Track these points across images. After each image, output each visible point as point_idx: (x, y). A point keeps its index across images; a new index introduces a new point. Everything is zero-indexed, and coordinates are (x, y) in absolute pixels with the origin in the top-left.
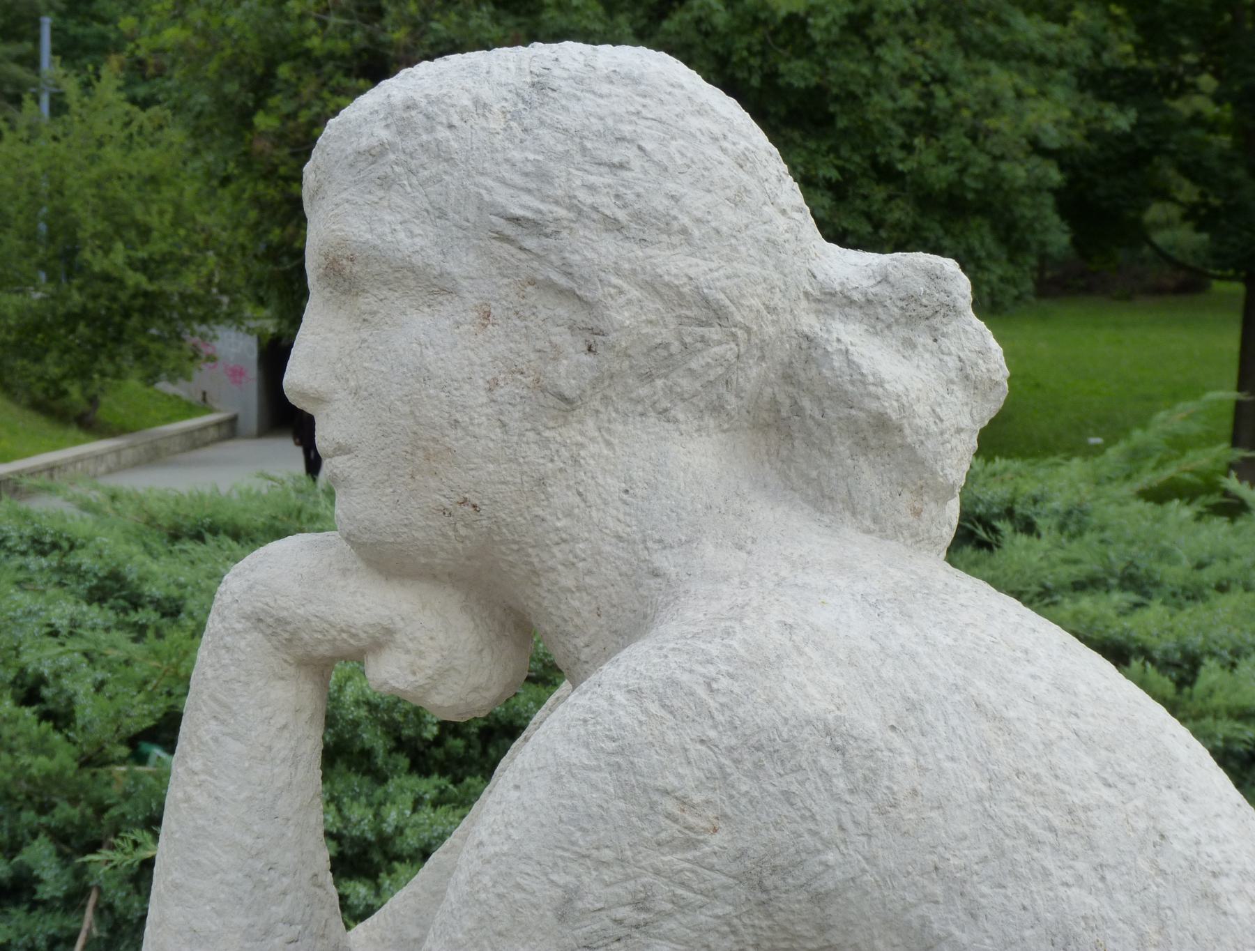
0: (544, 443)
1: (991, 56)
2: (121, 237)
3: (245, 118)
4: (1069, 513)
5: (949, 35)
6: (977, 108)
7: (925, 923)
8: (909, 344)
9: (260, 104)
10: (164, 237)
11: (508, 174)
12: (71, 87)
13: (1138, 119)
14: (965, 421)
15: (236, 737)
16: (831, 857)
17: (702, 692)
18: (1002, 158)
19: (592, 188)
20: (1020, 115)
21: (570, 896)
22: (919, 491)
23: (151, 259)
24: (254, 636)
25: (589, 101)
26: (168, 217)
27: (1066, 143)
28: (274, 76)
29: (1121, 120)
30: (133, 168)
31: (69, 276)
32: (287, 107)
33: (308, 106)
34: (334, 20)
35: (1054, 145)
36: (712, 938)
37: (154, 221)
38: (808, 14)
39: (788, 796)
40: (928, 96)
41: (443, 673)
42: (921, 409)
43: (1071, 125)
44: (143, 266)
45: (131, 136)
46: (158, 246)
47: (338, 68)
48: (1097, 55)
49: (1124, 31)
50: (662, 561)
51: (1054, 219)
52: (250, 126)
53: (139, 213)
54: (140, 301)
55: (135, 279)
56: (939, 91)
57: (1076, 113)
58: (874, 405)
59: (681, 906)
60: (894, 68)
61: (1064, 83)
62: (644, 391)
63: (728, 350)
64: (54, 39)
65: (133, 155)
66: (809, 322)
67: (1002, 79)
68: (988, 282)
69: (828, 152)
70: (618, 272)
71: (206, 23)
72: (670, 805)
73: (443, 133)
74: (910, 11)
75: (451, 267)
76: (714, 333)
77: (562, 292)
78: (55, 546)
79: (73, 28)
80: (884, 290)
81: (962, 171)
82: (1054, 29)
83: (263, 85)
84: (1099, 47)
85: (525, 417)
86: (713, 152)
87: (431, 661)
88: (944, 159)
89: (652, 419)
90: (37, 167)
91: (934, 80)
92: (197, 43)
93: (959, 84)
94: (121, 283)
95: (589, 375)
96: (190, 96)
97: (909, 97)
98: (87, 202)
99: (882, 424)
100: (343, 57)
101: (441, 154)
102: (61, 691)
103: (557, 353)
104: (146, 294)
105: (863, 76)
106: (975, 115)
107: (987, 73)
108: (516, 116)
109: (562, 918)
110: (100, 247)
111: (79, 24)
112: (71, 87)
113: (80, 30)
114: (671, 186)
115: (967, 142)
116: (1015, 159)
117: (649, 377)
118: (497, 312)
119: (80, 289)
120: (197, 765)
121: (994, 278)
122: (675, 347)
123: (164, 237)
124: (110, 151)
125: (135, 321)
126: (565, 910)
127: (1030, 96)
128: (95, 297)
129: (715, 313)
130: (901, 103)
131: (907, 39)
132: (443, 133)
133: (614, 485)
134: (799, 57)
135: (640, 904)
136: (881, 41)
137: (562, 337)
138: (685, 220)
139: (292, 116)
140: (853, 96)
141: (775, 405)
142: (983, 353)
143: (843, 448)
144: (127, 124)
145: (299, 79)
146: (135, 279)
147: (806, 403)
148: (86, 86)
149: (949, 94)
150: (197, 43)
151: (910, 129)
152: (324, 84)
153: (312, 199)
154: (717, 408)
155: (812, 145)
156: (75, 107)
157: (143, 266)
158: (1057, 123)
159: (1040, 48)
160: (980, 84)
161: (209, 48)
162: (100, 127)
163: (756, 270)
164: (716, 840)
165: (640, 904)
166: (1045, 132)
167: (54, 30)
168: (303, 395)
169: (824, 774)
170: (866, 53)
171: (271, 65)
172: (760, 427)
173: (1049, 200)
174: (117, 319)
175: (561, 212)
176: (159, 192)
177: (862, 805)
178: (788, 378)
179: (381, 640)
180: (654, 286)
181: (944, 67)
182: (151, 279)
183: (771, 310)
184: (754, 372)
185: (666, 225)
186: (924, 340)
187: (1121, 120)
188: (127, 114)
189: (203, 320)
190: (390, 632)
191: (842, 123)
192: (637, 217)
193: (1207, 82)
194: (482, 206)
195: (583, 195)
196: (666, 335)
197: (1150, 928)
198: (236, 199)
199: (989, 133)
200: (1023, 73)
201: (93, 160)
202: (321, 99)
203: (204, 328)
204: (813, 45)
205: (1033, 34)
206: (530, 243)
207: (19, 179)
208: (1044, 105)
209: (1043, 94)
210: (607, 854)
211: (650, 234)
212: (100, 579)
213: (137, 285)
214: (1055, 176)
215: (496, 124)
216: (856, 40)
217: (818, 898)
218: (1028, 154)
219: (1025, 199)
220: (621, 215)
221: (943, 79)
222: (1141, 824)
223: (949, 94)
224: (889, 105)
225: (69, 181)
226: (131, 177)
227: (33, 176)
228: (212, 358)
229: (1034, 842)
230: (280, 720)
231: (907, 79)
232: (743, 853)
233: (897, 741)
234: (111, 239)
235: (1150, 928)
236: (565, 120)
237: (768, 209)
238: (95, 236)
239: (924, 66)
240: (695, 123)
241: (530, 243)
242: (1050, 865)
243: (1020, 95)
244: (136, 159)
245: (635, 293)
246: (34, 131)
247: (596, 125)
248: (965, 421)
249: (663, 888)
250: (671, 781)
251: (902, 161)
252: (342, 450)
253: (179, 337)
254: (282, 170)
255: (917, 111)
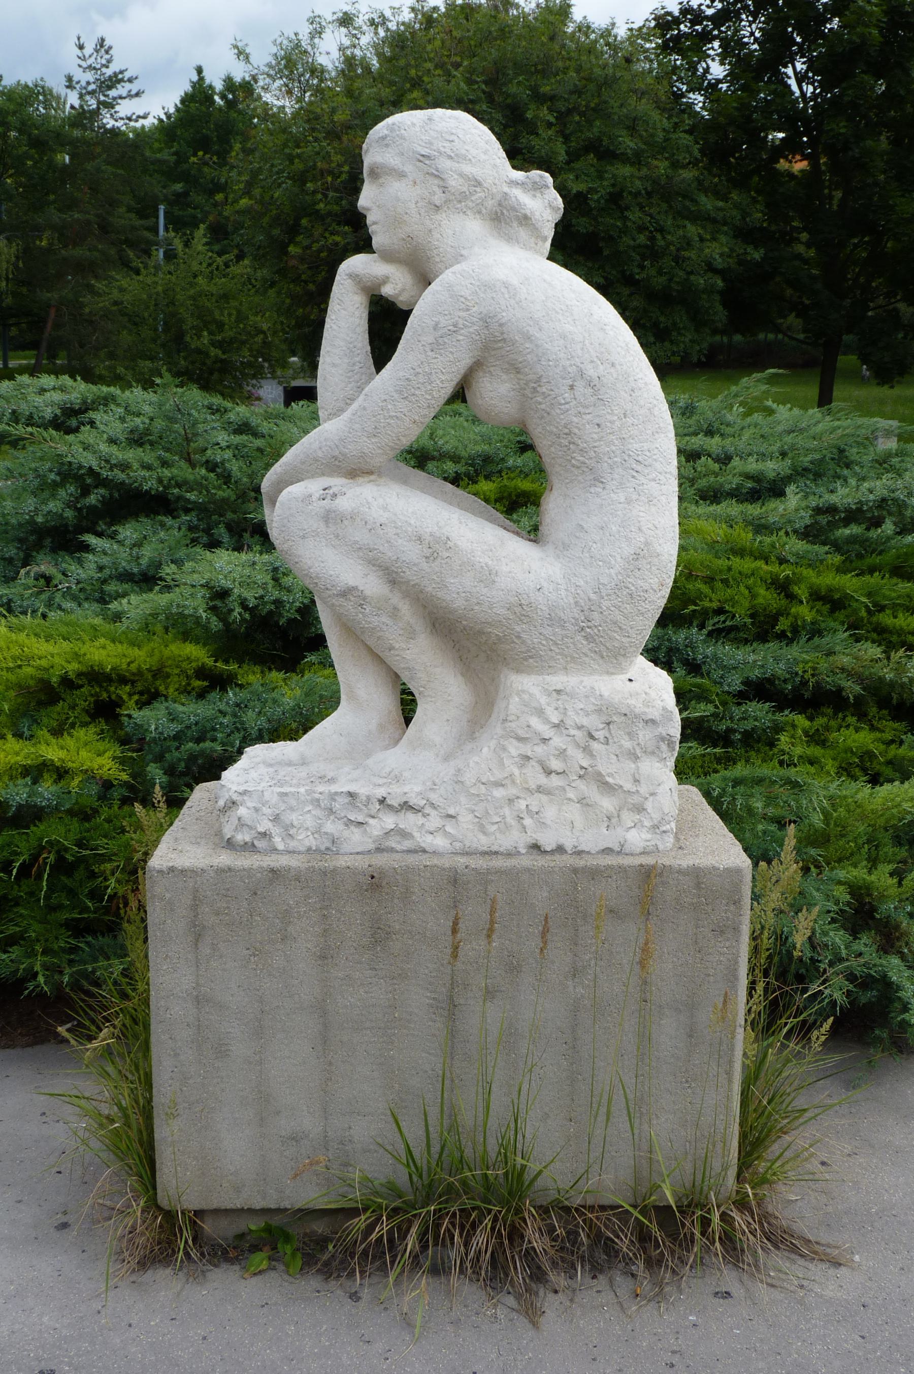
0: (431, 220)
1: (687, 218)
2: (208, 329)
3: (283, 248)
4: (687, 407)
5: (664, 206)
6: (678, 246)
7: (528, 331)
8: (535, 196)
9: (291, 241)
10: (231, 328)
11: (420, 143)
12: (178, 244)
13: (765, 254)
14: (550, 218)
15: (344, 309)
16: (504, 314)
17: (471, 272)
18: (692, 273)
19: (444, 147)
20: (701, 250)
21: (437, 324)
22: (537, 238)
23: (224, 340)
24: (349, 281)
25: (444, 123)
26: (233, 318)
27: (726, 265)
28: (299, 225)
29: (757, 255)
30: (213, 289)
31: (179, 351)
32: (306, 243)
33: (317, 241)
34: (331, 194)
35: (720, 267)
36: (473, 336)
37: (226, 319)
38: (588, 192)
39: (493, 298)
40: (652, 239)
41: (403, 290)
42: (537, 214)
43: (729, 256)
44: (220, 345)
45: (211, 272)
46: (229, 334)
47: (334, 220)
48: (744, 218)
49: (758, 207)
50: (464, 252)
51: (721, 308)
52: (286, 253)
53: (217, 315)
54: (219, 365)
55: (214, 352)
56: (659, 236)
57: (732, 250)
58: (523, 211)
59: (465, 326)
60: (634, 223)
61: (726, 233)
62: (459, 206)
63: (482, 195)
64: (165, 218)
65: (214, 281)
66: (506, 189)
67: (692, 230)
68: (684, 342)
69: (599, 269)
70: (451, 170)
71: (262, 197)
72: (463, 300)
73: (403, 132)
74: (643, 192)
75: (405, 169)
76: (478, 189)
77: (436, 176)
78: (218, 410)
79: (177, 212)
80: (528, 180)
81: (670, 280)
82: (721, 204)
83: (293, 230)
84: (745, 214)
85: (426, 212)
86: (478, 139)
87: (400, 286)
88: (660, 273)
89: (461, 214)
90: (160, 289)
91: (656, 230)
92: (257, 207)
93: (669, 233)
94: (207, 354)
95: (444, 199)
96: (254, 237)
97: (642, 239)
98: (188, 308)
99: (526, 217)
100: (336, 215)
101: (402, 138)
102: (225, 470)
103: (434, 193)
104: (222, 361)
105: (618, 227)
106: (678, 250)
107: (685, 227)
108: (423, 127)
109: (435, 329)
110: (195, 334)
111: (180, 210)
112: (178, 244)
113: (181, 213)
114: (466, 147)
115: (674, 264)
116: (699, 274)
117: (460, 202)
118: (418, 182)
119: (185, 358)
120: (333, 317)
121: (687, 340)
122: (468, 193)
123: (231, 328)
124: (200, 280)
125: (216, 376)
126: (436, 327)
127: (708, 240)
128: (193, 363)
129: (478, 184)
130: (638, 242)
131: (642, 207)
132: (403, 132)
133: (450, 232)
134: (583, 216)
135: (455, 326)
136: (627, 208)
137: (436, 189)
138: (470, 157)
139: (309, 247)
140: (611, 238)
141: (496, 213)
142: (555, 199)
143: (515, 224)
144: (210, 265)
145: (313, 227)
146: (214, 352)
147: (505, 211)
148: (187, 244)
149: (664, 238)
150: (257, 207)
151: (644, 257)
152: (326, 230)
153: (366, 153)
154: (480, 212)
155: (590, 264)
156: (181, 254)
157: (220, 345)
158: (721, 255)
159: (713, 214)
160: (681, 232)
161: (264, 211)
162: (195, 266)
163: (490, 172)
164: (474, 309)
165: (455, 326)
166: (715, 259)
167: (165, 213)
168: (363, 208)
169: (503, 293)
170: (620, 215)
171: (297, 219)
172: (492, 220)
173: (717, 297)
174: (206, 375)
175: (436, 153)
176: (228, 303)
177: (512, 302)
178: (500, 205)
179: (385, 280)
180: (461, 175)
181: (661, 223)
182: (224, 353)
183: (495, 184)
184: (490, 202)
185: (465, 158)
186: (539, 195)
187: (757, 255)
188: (211, 258)
189: (254, 376)
190: (388, 278)
191: (606, 252)
192: (457, 155)
193: (804, 236)
194: (413, 152)
195: (442, 149)
196: (465, 189)
197: (586, 335)
198: (279, 293)
199: (685, 259)
200: (704, 227)
201: (192, 285)
202: (325, 238)
203: (254, 382)
204: (591, 209)
205: (709, 207)
206: (427, 162)
207: (150, 297)
208: (715, 244)
209: (714, 239)
210: (446, 312)
211: (460, 160)
212: (240, 426)
213: (216, 356)
214: (720, 283)
215: (418, 129)
216: (614, 207)
217: (501, 325)
218: (706, 271)
219: (705, 296)
220: (452, 155)
221: (661, 230)
222: (586, 311)
223: (664, 238)
224: (632, 243)
225: (178, 297)
226: (212, 294)
227: (157, 294)
228: (259, 399)
229: (557, 313)
230: (357, 306)
231: (641, 229)
232: (481, 313)
233: (522, 286)
234: (202, 330)
235: (586, 335)
236: (437, 128)
237: (495, 157)
238: (193, 328)
239: (650, 222)
240: (474, 131)
241: (427, 162)
242: (561, 318)
243: (702, 240)
244: (215, 284)
245: (456, 177)
246: (157, 268)
247: (446, 130)
248: (550, 218)
249: (461, 322)
250: (463, 293)
251: (638, 274)
252: (375, 223)
253: (241, 387)
254: (303, 277)
255: (646, 246)
